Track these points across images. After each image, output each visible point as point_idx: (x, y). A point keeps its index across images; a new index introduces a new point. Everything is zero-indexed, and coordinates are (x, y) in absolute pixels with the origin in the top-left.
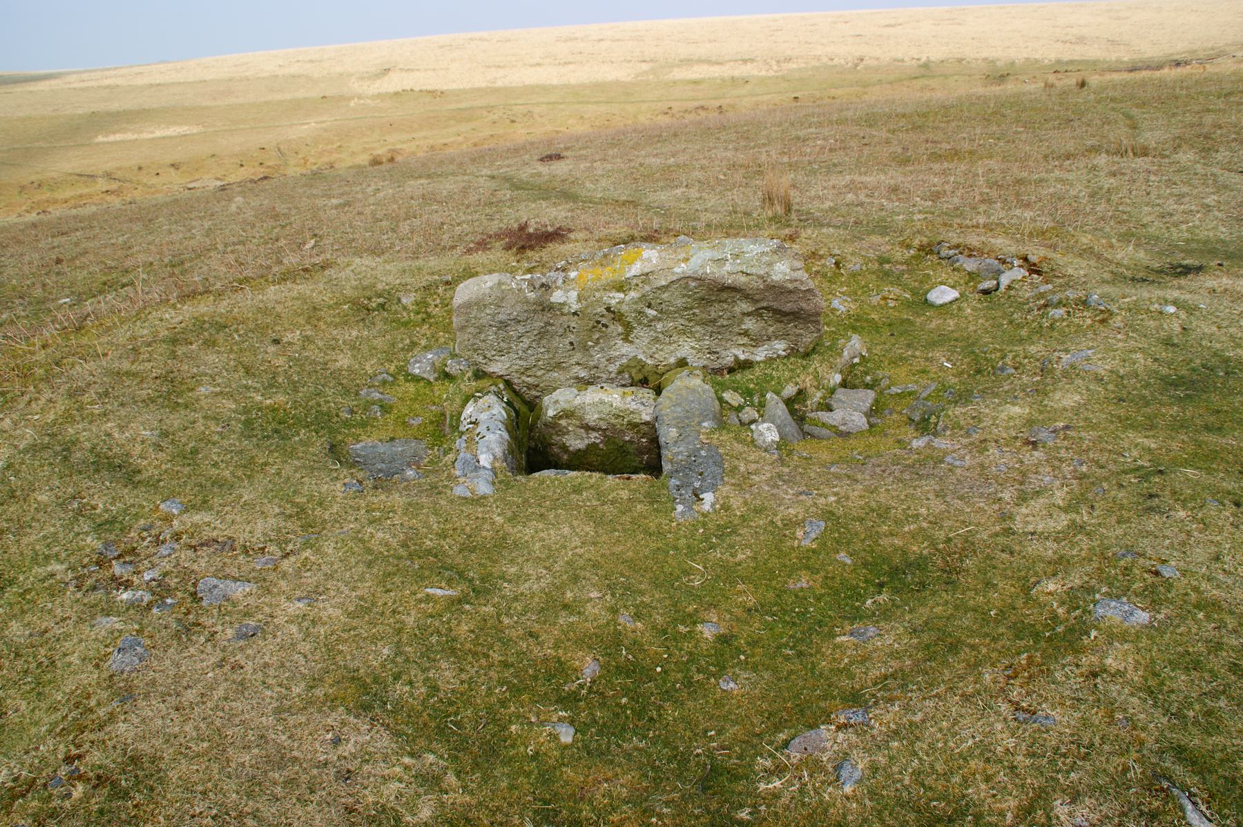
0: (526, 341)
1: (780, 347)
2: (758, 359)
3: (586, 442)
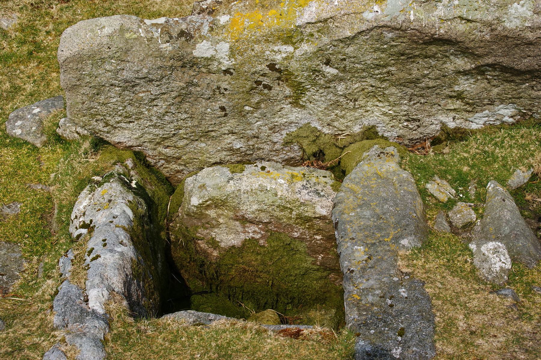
0: (162, 106)
1: (507, 112)
2: (474, 126)
3: (243, 237)
